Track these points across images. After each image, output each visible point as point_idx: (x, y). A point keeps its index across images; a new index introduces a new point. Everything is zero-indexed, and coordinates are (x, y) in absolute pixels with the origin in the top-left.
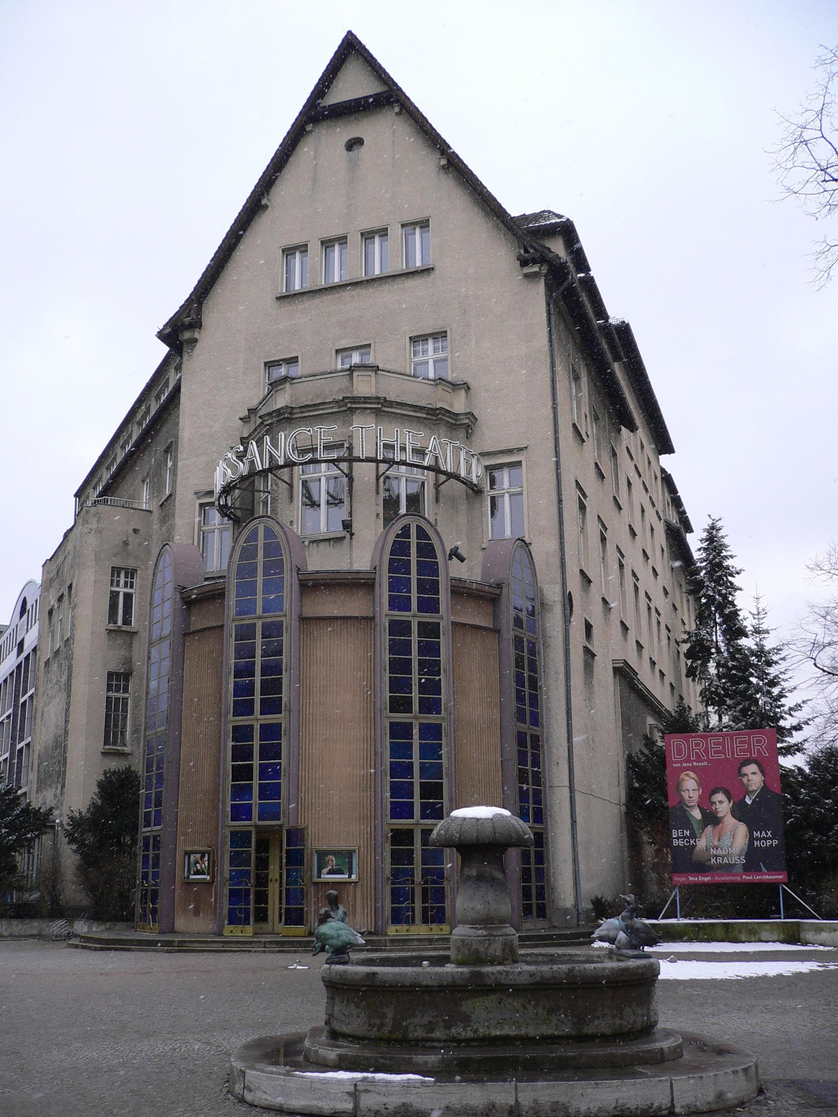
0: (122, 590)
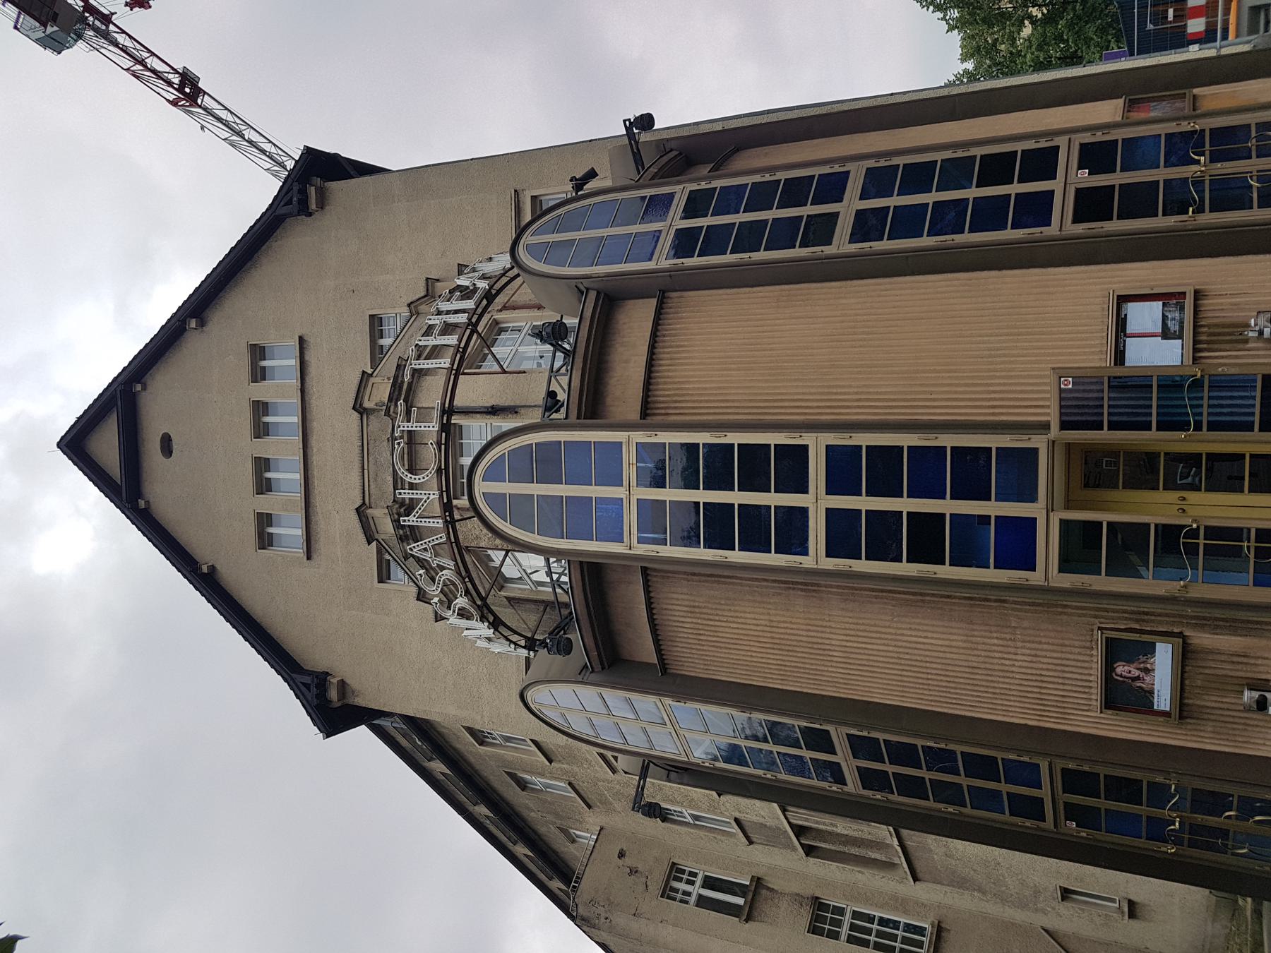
0: (697, 890)
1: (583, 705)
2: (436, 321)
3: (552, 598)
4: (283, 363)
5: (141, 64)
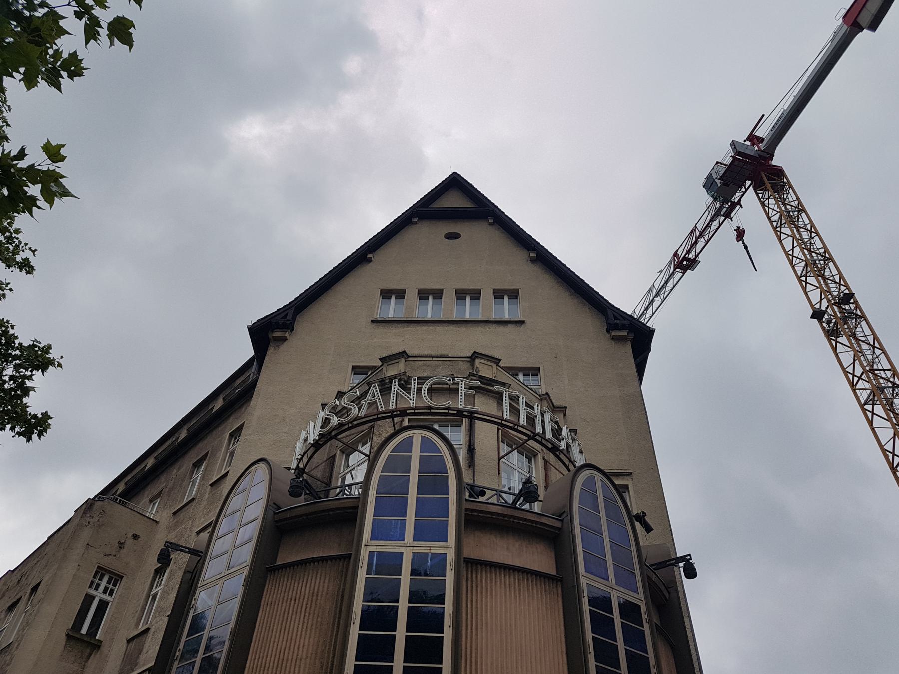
0: (99, 595)
1: (250, 507)
2: (537, 410)
3: (333, 485)
4: (506, 310)
5: (699, 235)
